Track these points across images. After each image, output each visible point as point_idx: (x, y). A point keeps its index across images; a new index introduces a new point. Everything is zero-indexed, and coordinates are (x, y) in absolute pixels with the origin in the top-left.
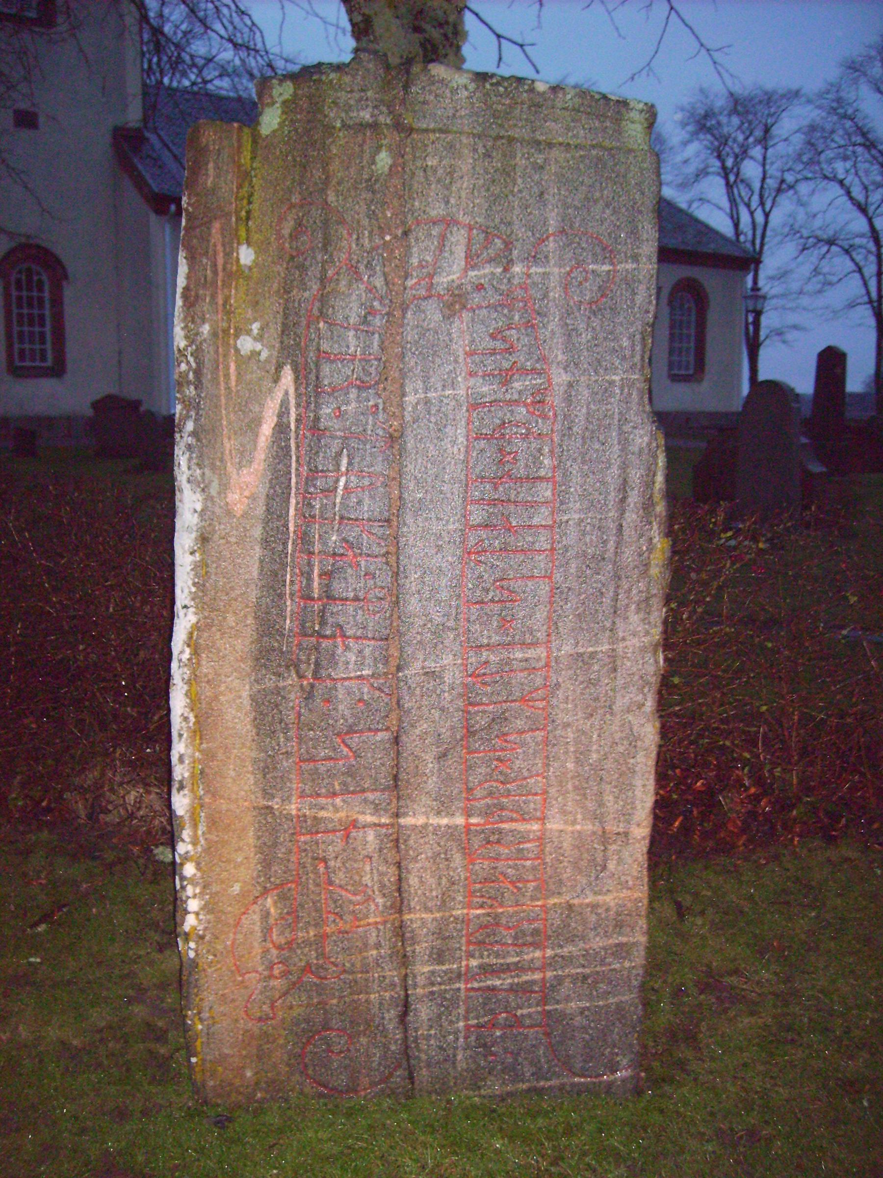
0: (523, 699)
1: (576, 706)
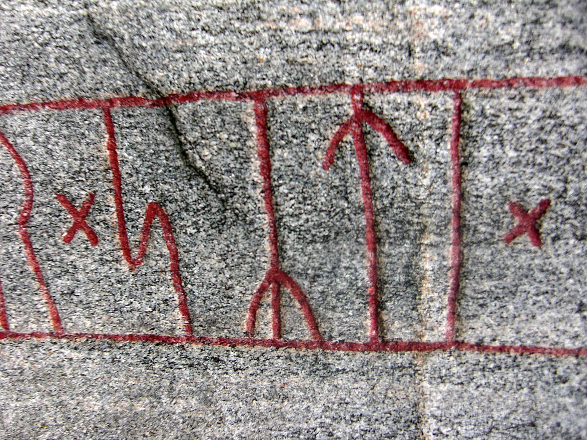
0: (279, 278)
1: (258, 418)
